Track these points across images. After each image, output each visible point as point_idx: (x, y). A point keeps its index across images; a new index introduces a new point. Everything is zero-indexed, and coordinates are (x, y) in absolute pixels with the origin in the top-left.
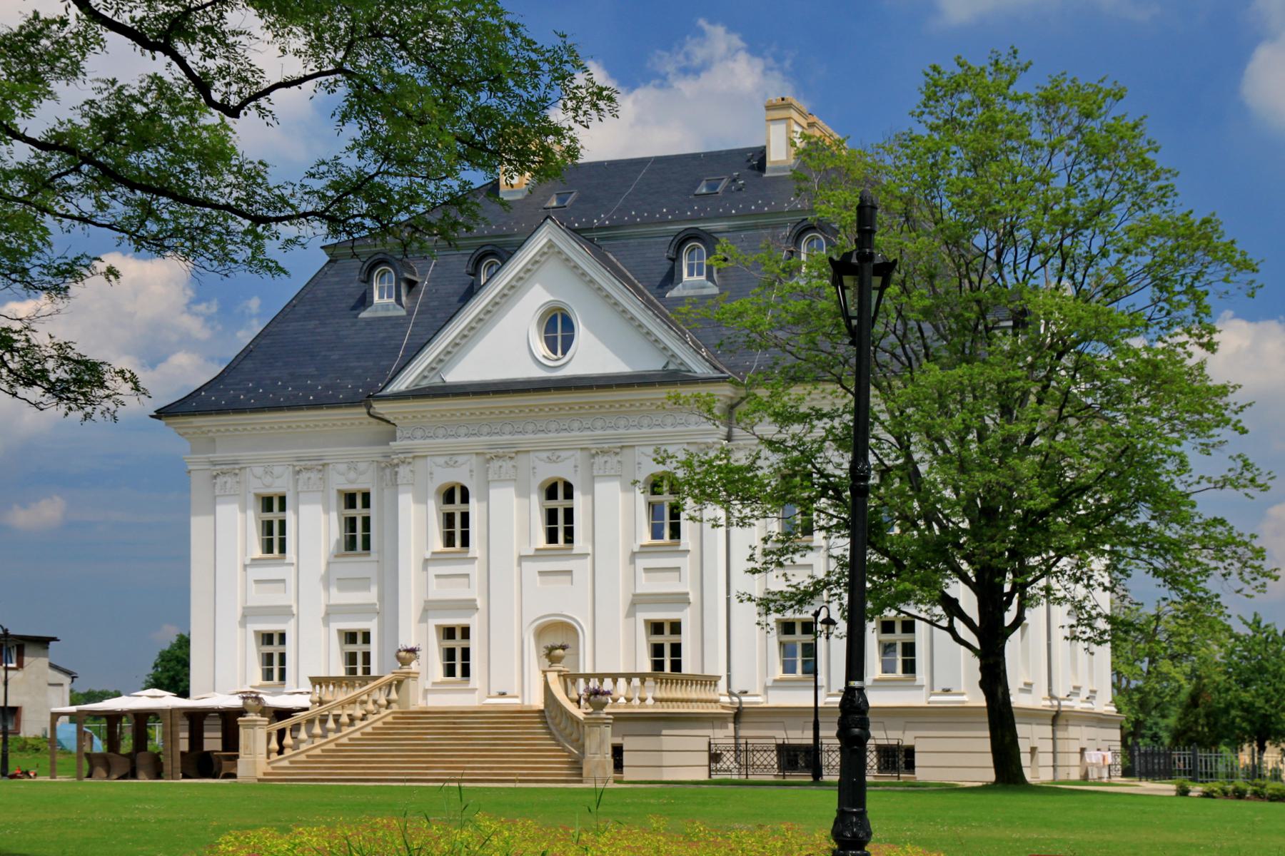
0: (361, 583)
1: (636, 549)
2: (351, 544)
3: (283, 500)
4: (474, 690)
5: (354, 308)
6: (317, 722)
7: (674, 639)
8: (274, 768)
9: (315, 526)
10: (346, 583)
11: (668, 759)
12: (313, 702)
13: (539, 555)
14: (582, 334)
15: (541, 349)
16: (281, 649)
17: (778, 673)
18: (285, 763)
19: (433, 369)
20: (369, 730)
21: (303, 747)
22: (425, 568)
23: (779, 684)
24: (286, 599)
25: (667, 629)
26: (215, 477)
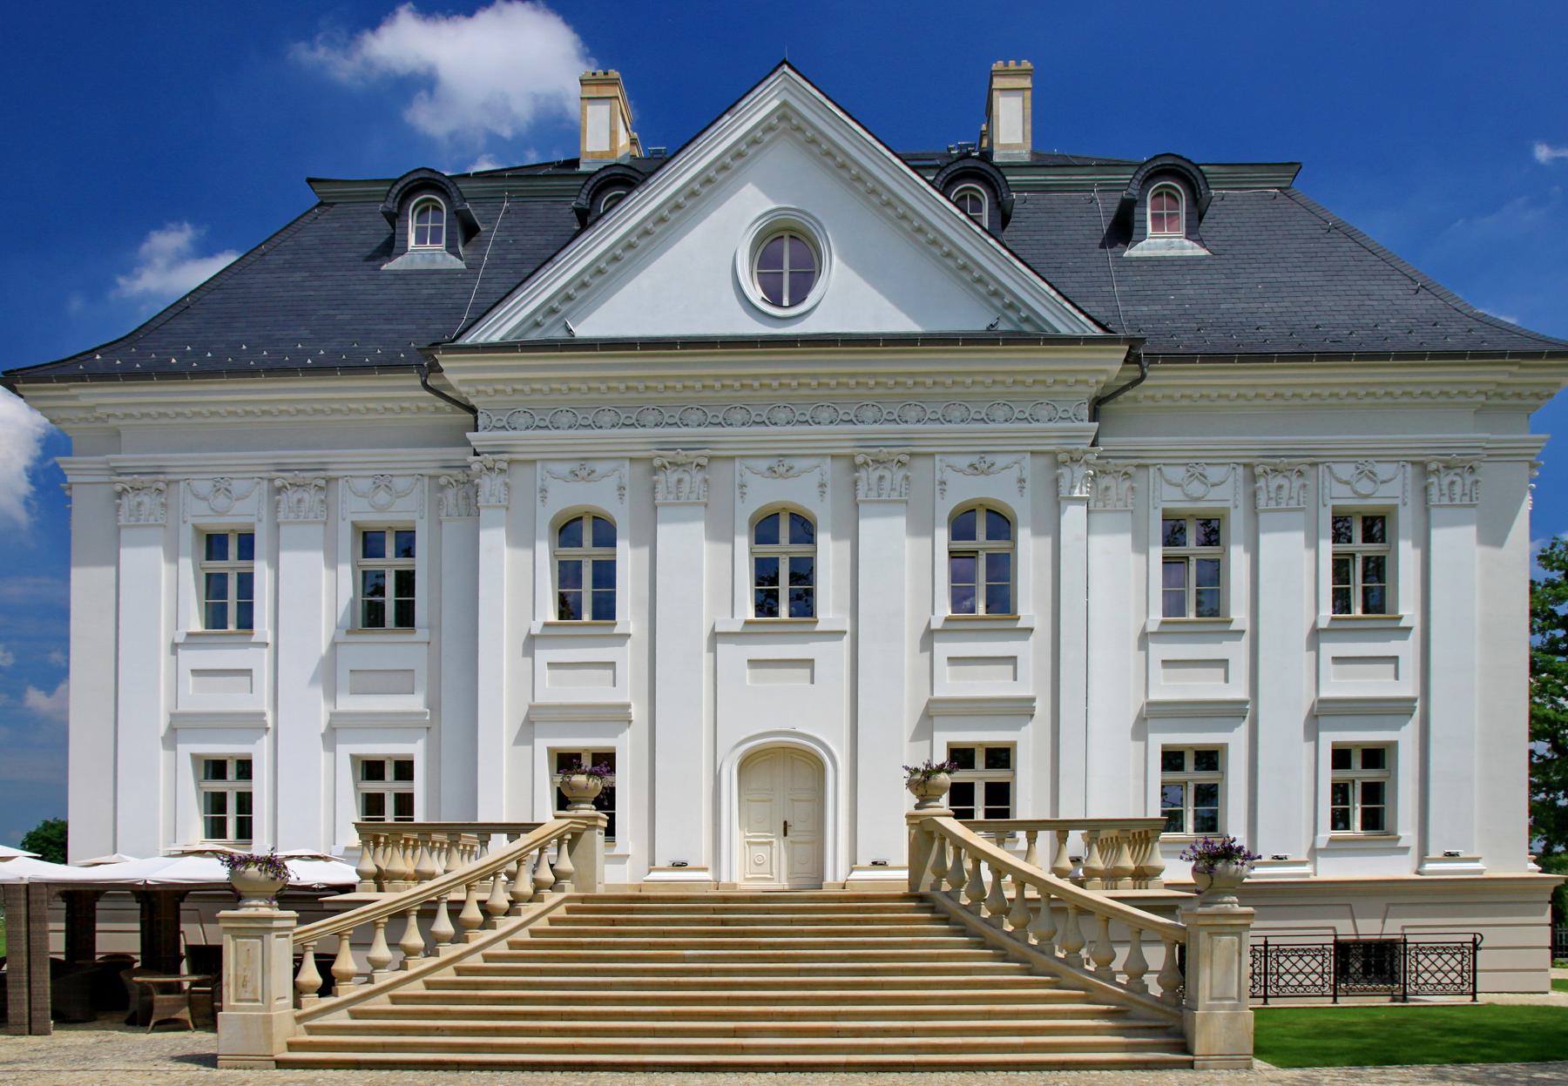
0: (400, 681)
2: (373, 617)
4: (623, 858)
5: (370, 258)
6: (413, 920)
7: (242, 786)
9: (308, 588)
10: (366, 680)
12: (363, 875)
13: (746, 634)
15: (756, 294)
19: (553, 311)
23: (1335, 848)
24: (260, 701)
26: (119, 495)
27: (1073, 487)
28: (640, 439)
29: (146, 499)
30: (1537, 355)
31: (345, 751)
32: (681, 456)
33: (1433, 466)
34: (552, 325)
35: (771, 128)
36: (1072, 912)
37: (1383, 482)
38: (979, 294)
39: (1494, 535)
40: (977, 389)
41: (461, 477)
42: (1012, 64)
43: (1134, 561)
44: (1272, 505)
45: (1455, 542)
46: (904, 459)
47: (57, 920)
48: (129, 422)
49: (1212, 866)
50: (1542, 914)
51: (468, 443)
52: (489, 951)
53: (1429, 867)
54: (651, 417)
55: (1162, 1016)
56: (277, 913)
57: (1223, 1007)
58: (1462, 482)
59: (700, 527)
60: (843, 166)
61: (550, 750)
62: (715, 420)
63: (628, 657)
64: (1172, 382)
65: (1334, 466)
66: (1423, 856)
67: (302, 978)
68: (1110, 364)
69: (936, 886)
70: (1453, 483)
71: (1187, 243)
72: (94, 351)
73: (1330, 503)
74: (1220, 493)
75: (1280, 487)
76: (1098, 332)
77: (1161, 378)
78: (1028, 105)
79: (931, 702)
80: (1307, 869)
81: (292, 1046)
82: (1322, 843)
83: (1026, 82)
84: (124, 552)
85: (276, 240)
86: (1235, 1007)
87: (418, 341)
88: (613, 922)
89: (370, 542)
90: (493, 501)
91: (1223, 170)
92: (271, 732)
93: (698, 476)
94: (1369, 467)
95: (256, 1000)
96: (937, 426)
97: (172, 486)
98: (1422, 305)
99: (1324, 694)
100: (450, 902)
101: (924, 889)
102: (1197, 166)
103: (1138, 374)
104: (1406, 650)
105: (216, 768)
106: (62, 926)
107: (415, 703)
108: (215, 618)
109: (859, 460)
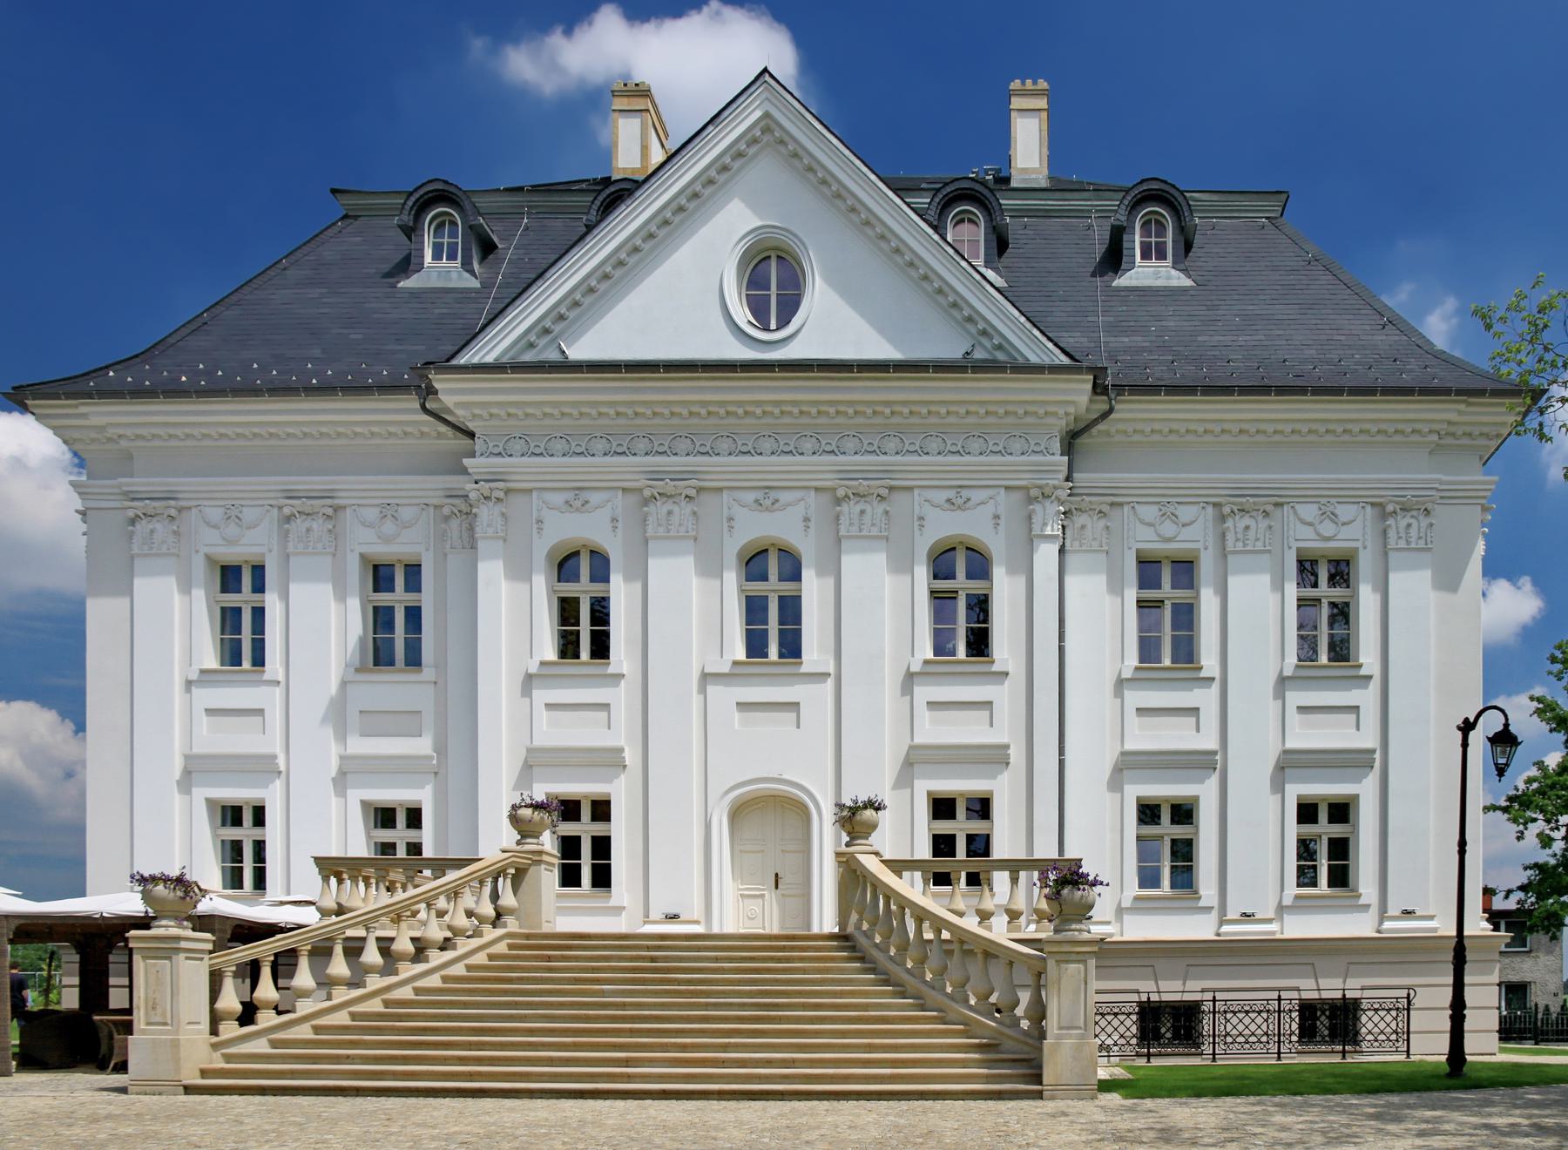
2: (381, 656)
3: (259, 571)
4: (619, 910)
6: (338, 949)
7: (599, 829)
8: (228, 1058)
9: (317, 622)
10: (377, 722)
14: (818, 296)
15: (742, 315)
16: (256, 833)
18: (261, 1046)
19: (547, 331)
20: (459, 970)
21: (304, 1007)
23: (1300, 905)
25: (586, 812)
26: (133, 522)
27: (1045, 524)
28: (631, 468)
29: (158, 526)
30: (1481, 393)
31: (356, 796)
32: (669, 487)
33: (1390, 508)
35: (755, 141)
36: (980, 956)
40: (952, 420)
41: (464, 508)
42: (1029, 82)
43: (1108, 602)
44: (1240, 546)
45: (1412, 586)
46: (884, 492)
47: (70, 975)
48: (140, 443)
49: (1058, 893)
50: (1491, 972)
51: (464, 471)
52: (419, 984)
53: (1387, 925)
54: (642, 445)
55: (1026, 1049)
56: (190, 934)
57: (1070, 1036)
58: (1418, 524)
60: (824, 182)
62: (703, 450)
63: (621, 698)
64: (1140, 416)
65: (1298, 507)
67: (220, 1005)
68: (1077, 394)
69: (858, 927)
70: (1409, 525)
71: (1174, 272)
72: (107, 367)
73: (1295, 545)
74: (1191, 533)
75: (1247, 528)
76: (1065, 360)
77: (1132, 412)
78: (1045, 127)
79: (912, 748)
80: (1274, 927)
81: (204, 1073)
82: (1287, 901)
83: (1042, 103)
84: (137, 582)
85: (299, 254)
86: (1082, 1037)
87: (416, 360)
88: (549, 959)
89: (381, 576)
90: (490, 531)
91: (1215, 197)
92: (283, 776)
93: (688, 508)
94: (1331, 508)
95: (165, 1024)
96: (915, 458)
97: (184, 514)
98: (1386, 340)
100: (378, 939)
101: (850, 929)
102: (1182, 192)
103: (1106, 407)
104: (1367, 698)
105: (233, 815)
106: (76, 981)
107: (422, 746)
108: (232, 655)
109: (841, 493)
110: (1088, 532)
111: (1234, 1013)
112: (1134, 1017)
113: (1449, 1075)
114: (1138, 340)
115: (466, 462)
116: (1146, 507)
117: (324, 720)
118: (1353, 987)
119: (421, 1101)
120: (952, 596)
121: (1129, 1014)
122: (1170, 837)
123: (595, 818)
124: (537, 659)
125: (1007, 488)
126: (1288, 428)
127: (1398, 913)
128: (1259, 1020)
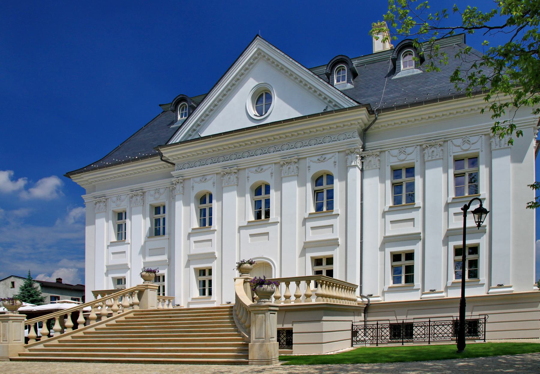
1: (307, 216)
8: (30, 350)
9: (139, 225)
10: (154, 252)
11: (326, 337)
14: (276, 100)
15: (253, 112)
17: (391, 283)
19: (195, 130)
22: (189, 238)
23: (391, 290)
25: (324, 262)
27: (352, 162)
28: (217, 167)
34: (195, 135)
35: (256, 58)
37: (473, 144)
38: (320, 99)
39: (518, 158)
45: (503, 164)
49: (255, 288)
51: (172, 177)
53: (491, 291)
57: (259, 341)
58: (437, 150)
59: (235, 193)
61: (312, 258)
65: (453, 141)
66: (490, 287)
68: (362, 115)
73: (453, 155)
74: (411, 157)
75: (433, 151)
76: (356, 104)
77: (385, 118)
81: (20, 355)
94: (404, 150)
99: (450, 227)
103: (374, 118)
110: (373, 162)
111: (438, 326)
112: (451, 326)
113: (458, 352)
114: (397, 94)
115: (172, 173)
116: (393, 151)
117: (139, 254)
118: (408, 319)
119: (54, 363)
120: (322, 191)
121: (448, 325)
122: (403, 267)
123: (327, 264)
124: (308, 212)
125: (339, 152)
126: (448, 113)
127: (496, 286)
128: (421, 329)
